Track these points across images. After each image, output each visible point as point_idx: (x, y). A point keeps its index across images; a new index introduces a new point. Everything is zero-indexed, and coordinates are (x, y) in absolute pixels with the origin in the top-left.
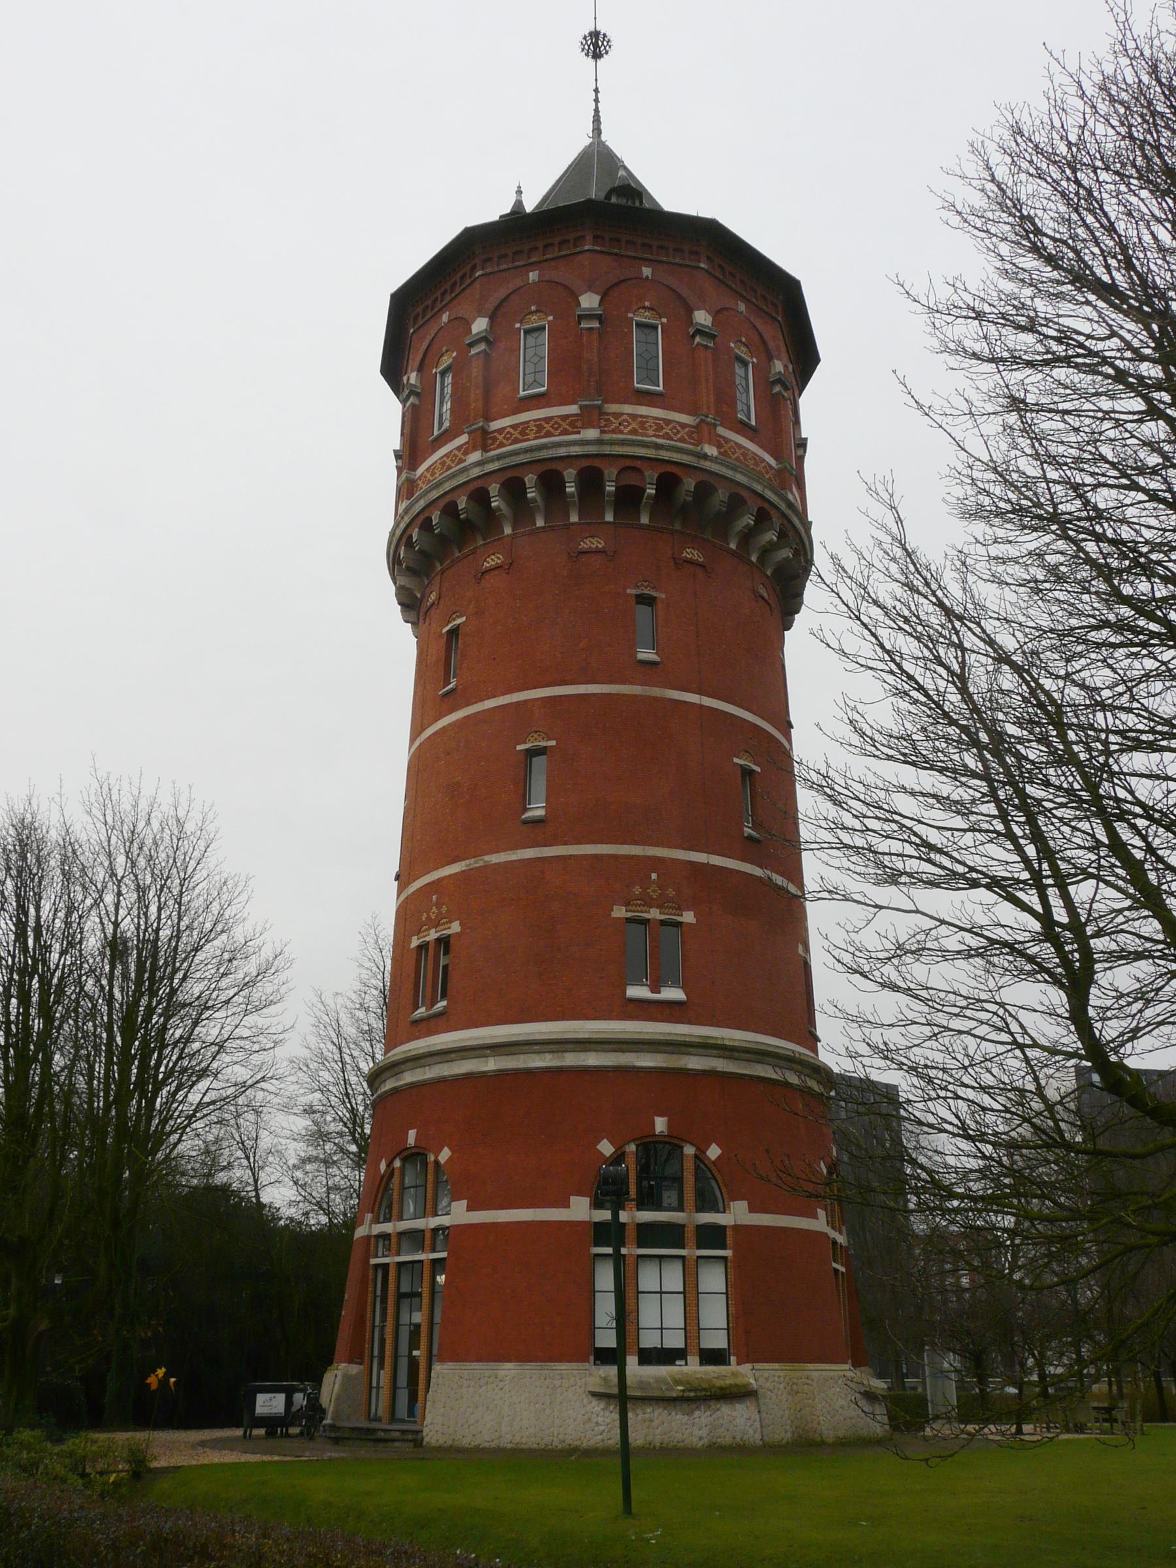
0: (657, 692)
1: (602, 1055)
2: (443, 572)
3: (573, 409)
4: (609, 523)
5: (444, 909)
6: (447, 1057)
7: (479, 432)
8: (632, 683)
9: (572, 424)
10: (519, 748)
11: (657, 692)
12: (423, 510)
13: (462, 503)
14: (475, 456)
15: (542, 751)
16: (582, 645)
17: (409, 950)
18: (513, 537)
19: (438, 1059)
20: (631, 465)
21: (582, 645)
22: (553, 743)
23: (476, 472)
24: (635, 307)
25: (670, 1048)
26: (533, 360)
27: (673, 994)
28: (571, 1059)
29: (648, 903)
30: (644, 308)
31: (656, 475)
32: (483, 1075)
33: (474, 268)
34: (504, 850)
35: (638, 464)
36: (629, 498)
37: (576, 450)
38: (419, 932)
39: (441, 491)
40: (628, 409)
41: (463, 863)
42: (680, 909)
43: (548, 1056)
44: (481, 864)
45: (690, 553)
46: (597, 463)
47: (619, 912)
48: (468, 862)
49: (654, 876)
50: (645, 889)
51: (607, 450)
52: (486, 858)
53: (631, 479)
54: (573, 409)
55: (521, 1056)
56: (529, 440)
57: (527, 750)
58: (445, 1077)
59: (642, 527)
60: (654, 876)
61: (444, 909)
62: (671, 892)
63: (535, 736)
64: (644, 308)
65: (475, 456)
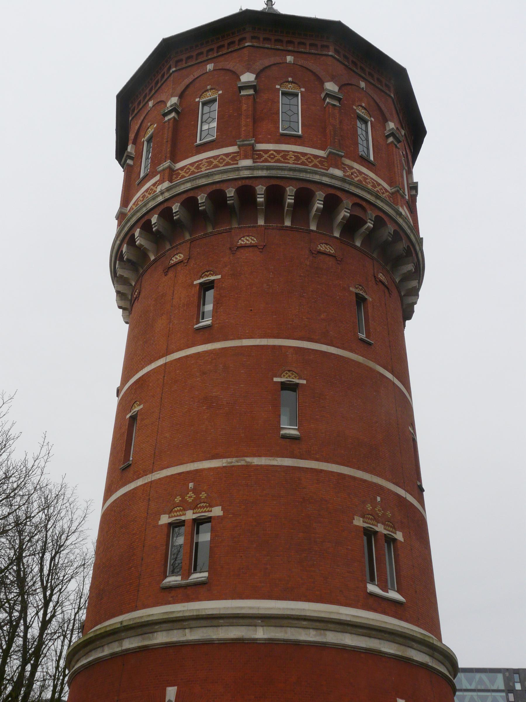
0: (371, 364)
1: (356, 637)
2: (192, 241)
3: (321, 153)
4: (336, 237)
5: (203, 495)
6: (215, 622)
7: (167, 171)
8: (357, 354)
9: (321, 162)
10: (275, 379)
11: (371, 364)
12: (166, 200)
13: (176, 208)
14: (166, 184)
15: (292, 387)
16: (322, 316)
17: (157, 526)
18: (266, 228)
19: (204, 623)
20: (360, 204)
21: (322, 316)
22: (304, 382)
23: (246, 173)
24: (357, 104)
25: (401, 640)
26: (292, 113)
27: (393, 595)
28: (332, 637)
29: (377, 519)
30: (361, 106)
31: (374, 216)
32: (253, 643)
33: (170, 68)
34: (266, 455)
35: (364, 204)
36: (352, 226)
37: (326, 180)
38: (171, 512)
39: (210, 180)
40: (356, 166)
41: (224, 460)
42: (395, 529)
43: (312, 632)
44: (243, 463)
45: (381, 276)
46: (339, 194)
47: (359, 522)
48: (229, 460)
49: (379, 499)
50: (374, 508)
51: (347, 187)
52: (248, 459)
53: (358, 213)
54: (321, 153)
55: (289, 629)
56: (289, 163)
57: (282, 383)
58: (213, 640)
59: (355, 247)
60: (379, 499)
61: (203, 495)
62: (389, 514)
63: (289, 373)
64: (361, 106)
65: (166, 184)
